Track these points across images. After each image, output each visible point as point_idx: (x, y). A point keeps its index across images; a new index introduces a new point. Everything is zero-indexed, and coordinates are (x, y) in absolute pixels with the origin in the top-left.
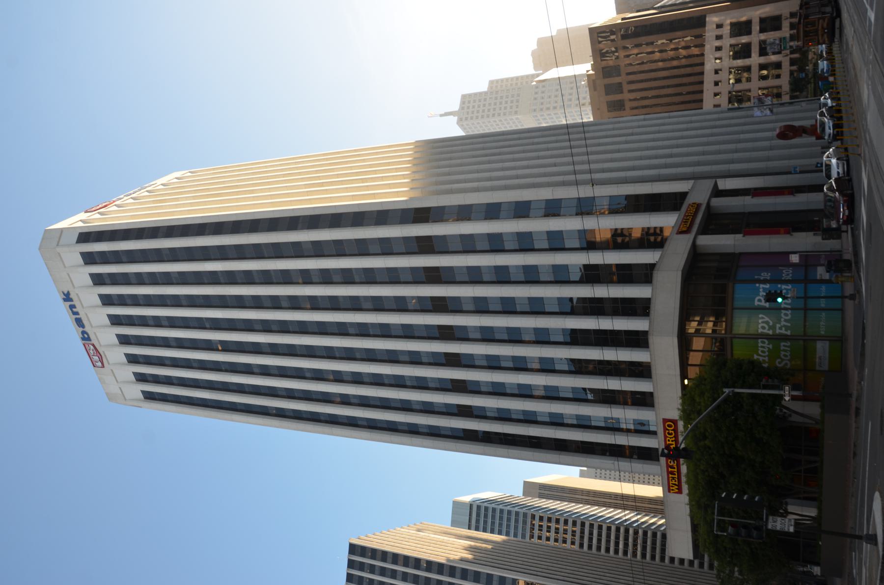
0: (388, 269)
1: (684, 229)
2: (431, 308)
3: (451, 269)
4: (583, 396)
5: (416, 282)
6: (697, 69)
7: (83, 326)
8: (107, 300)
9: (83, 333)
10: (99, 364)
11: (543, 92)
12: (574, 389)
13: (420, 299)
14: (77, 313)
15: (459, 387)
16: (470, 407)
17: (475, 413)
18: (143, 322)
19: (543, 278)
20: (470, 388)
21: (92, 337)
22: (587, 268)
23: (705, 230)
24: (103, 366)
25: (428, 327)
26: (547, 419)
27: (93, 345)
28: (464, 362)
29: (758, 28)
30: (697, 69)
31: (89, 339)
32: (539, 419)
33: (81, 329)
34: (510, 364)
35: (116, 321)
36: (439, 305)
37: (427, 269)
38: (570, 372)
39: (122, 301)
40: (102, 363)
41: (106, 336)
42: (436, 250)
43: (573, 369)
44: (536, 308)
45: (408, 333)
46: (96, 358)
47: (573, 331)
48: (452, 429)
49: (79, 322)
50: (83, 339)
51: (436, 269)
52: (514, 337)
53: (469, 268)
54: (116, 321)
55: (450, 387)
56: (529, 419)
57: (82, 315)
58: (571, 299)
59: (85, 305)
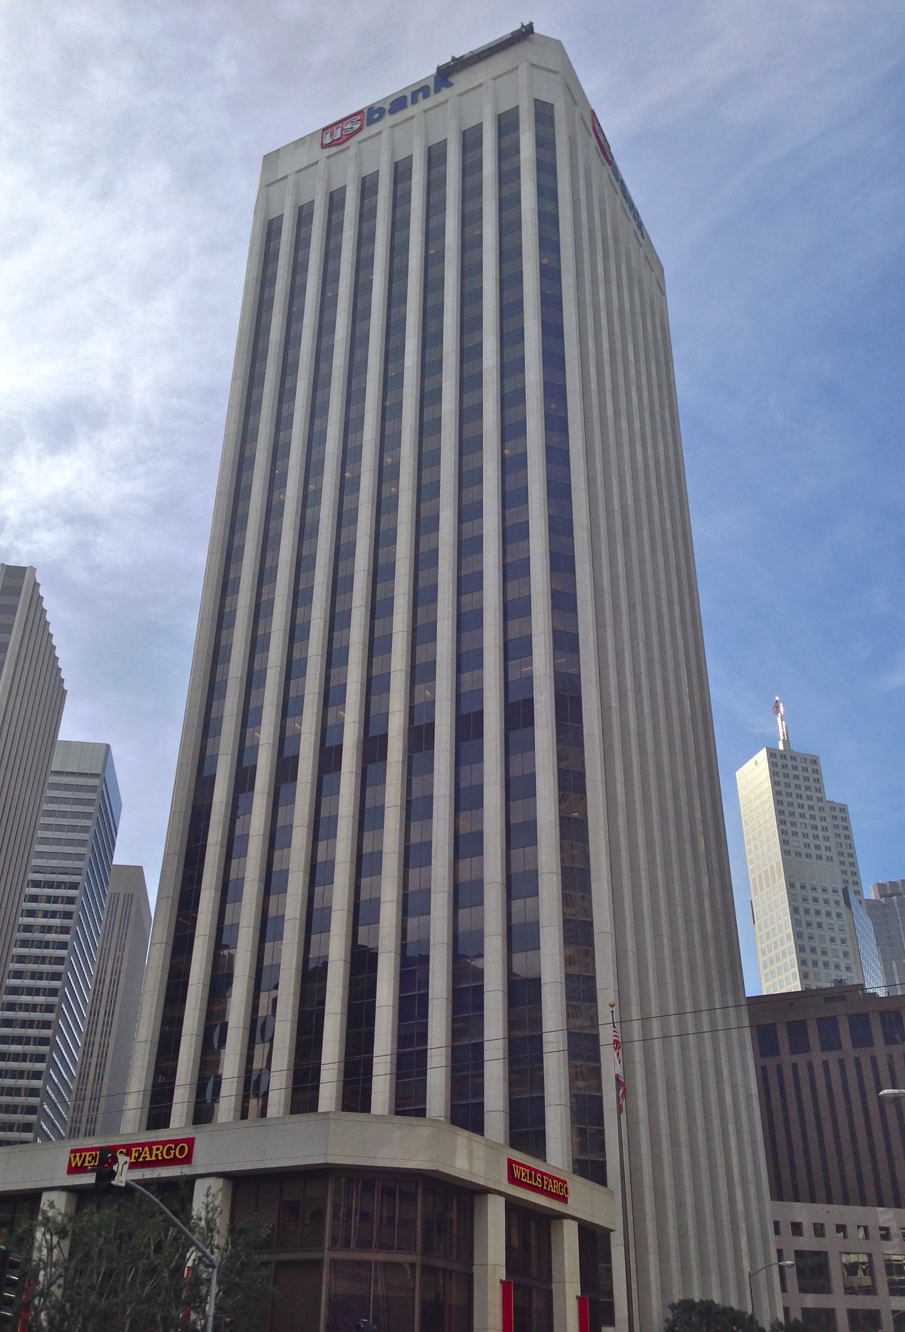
0: (481, 650)
1: (516, 1174)
2: (464, 712)
3: (479, 758)
4: (265, 983)
5: (411, 710)
6: (821, 1193)
7: (392, 111)
8: (435, 157)
9: (381, 111)
10: (328, 140)
11: (828, 914)
12: (276, 967)
13: (431, 705)
14: (414, 101)
15: (286, 769)
16: (252, 788)
17: (242, 797)
18: (471, 193)
19: (517, 904)
20: (326, 777)
21: (374, 128)
22: (535, 984)
23: (516, 1211)
24: (324, 146)
25: (385, 718)
26: (272, 912)
27: (360, 130)
28: (371, 767)
29: (859, 1306)
30: (821, 1193)
31: (371, 121)
32: (273, 899)
33: (387, 107)
34: (321, 857)
35: (401, 172)
36: (420, 737)
37: (479, 716)
38: (306, 960)
39: (471, 168)
40: (329, 145)
41: (377, 154)
42: (512, 734)
43: (311, 966)
44: (466, 894)
45: (375, 685)
46: (338, 133)
47: (425, 960)
48: (215, 758)
49: (399, 103)
50: (371, 110)
51: (529, 721)
52: (466, 845)
53: (481, 787)
54: (471, 141)
55: (286, 754)
56: (228, 891)
57: (411, 110)
58: (481, 955)
59: (428, 114)
